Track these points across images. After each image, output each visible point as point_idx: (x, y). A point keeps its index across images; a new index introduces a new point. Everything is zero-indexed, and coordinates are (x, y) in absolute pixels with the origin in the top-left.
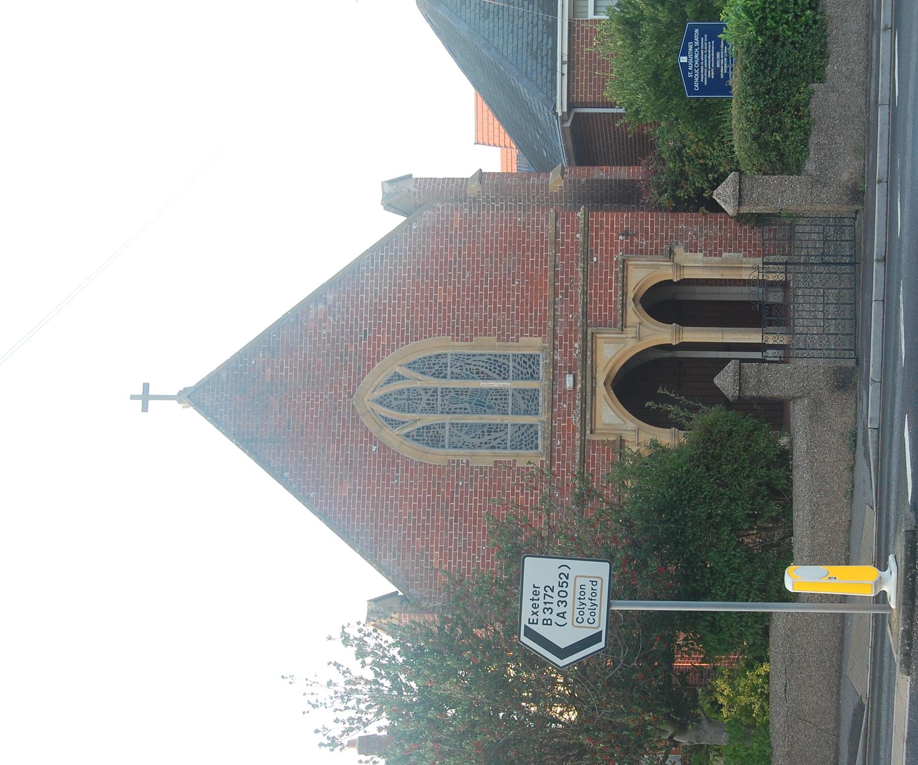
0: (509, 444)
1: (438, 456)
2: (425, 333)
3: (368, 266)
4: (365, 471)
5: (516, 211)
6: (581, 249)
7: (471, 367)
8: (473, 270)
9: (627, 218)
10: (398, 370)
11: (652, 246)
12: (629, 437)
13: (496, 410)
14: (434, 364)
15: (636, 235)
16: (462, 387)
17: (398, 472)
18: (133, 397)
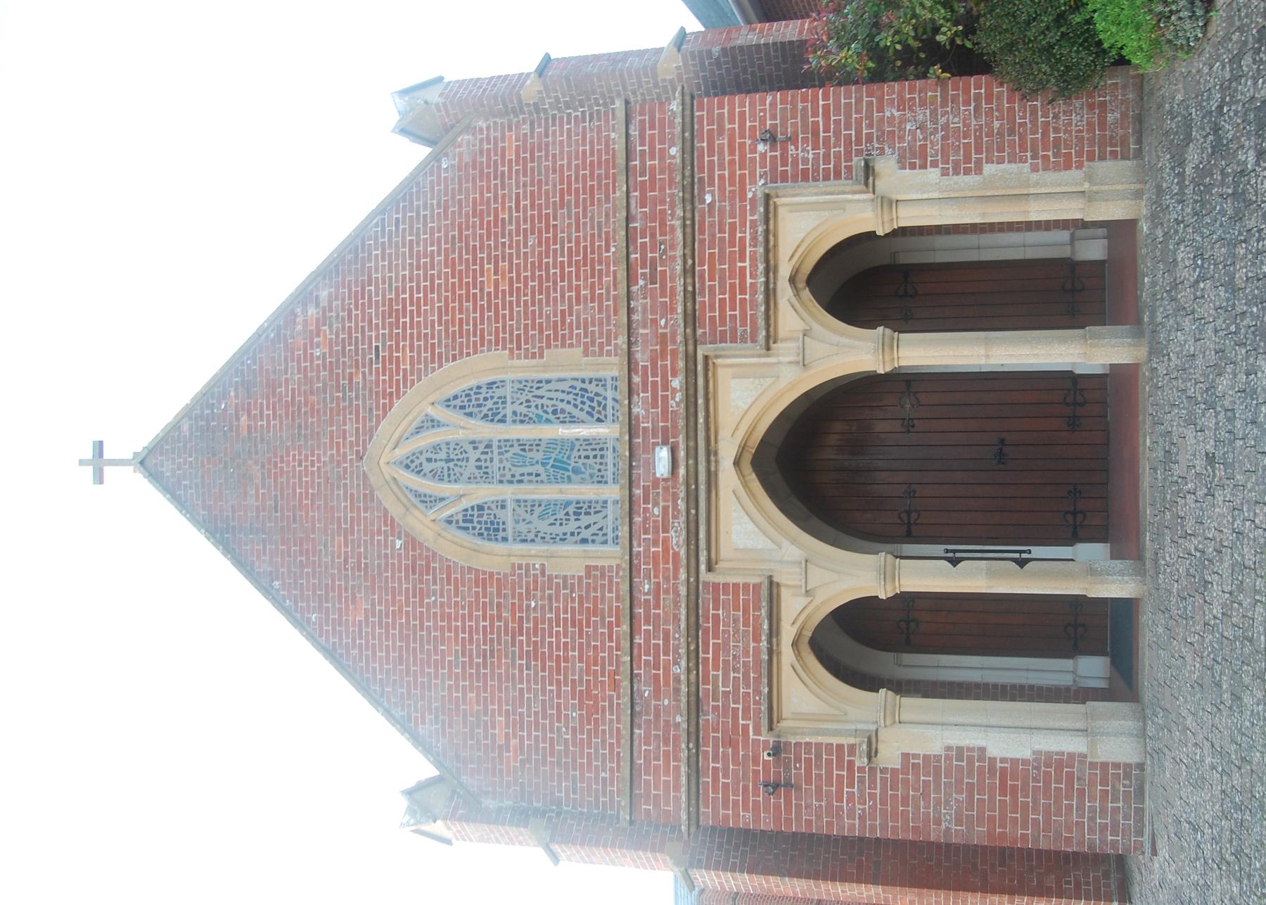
0: (610, 536)
1: (496, 557)
2: (468, 348)
3: (376, 239)
4: (387, 582)
5: (607, 121)
6: (678, 178)
7: (544, 401)
8: (540, 232)
9: (773, 105)
10: (430, 411)
11: (827, 159)
12: (788, 577)
13: (587, 476)
14: (486, 399)
15: (793, 139)
16: (532, 437)
17: (435, 583)
18: (82, 463)
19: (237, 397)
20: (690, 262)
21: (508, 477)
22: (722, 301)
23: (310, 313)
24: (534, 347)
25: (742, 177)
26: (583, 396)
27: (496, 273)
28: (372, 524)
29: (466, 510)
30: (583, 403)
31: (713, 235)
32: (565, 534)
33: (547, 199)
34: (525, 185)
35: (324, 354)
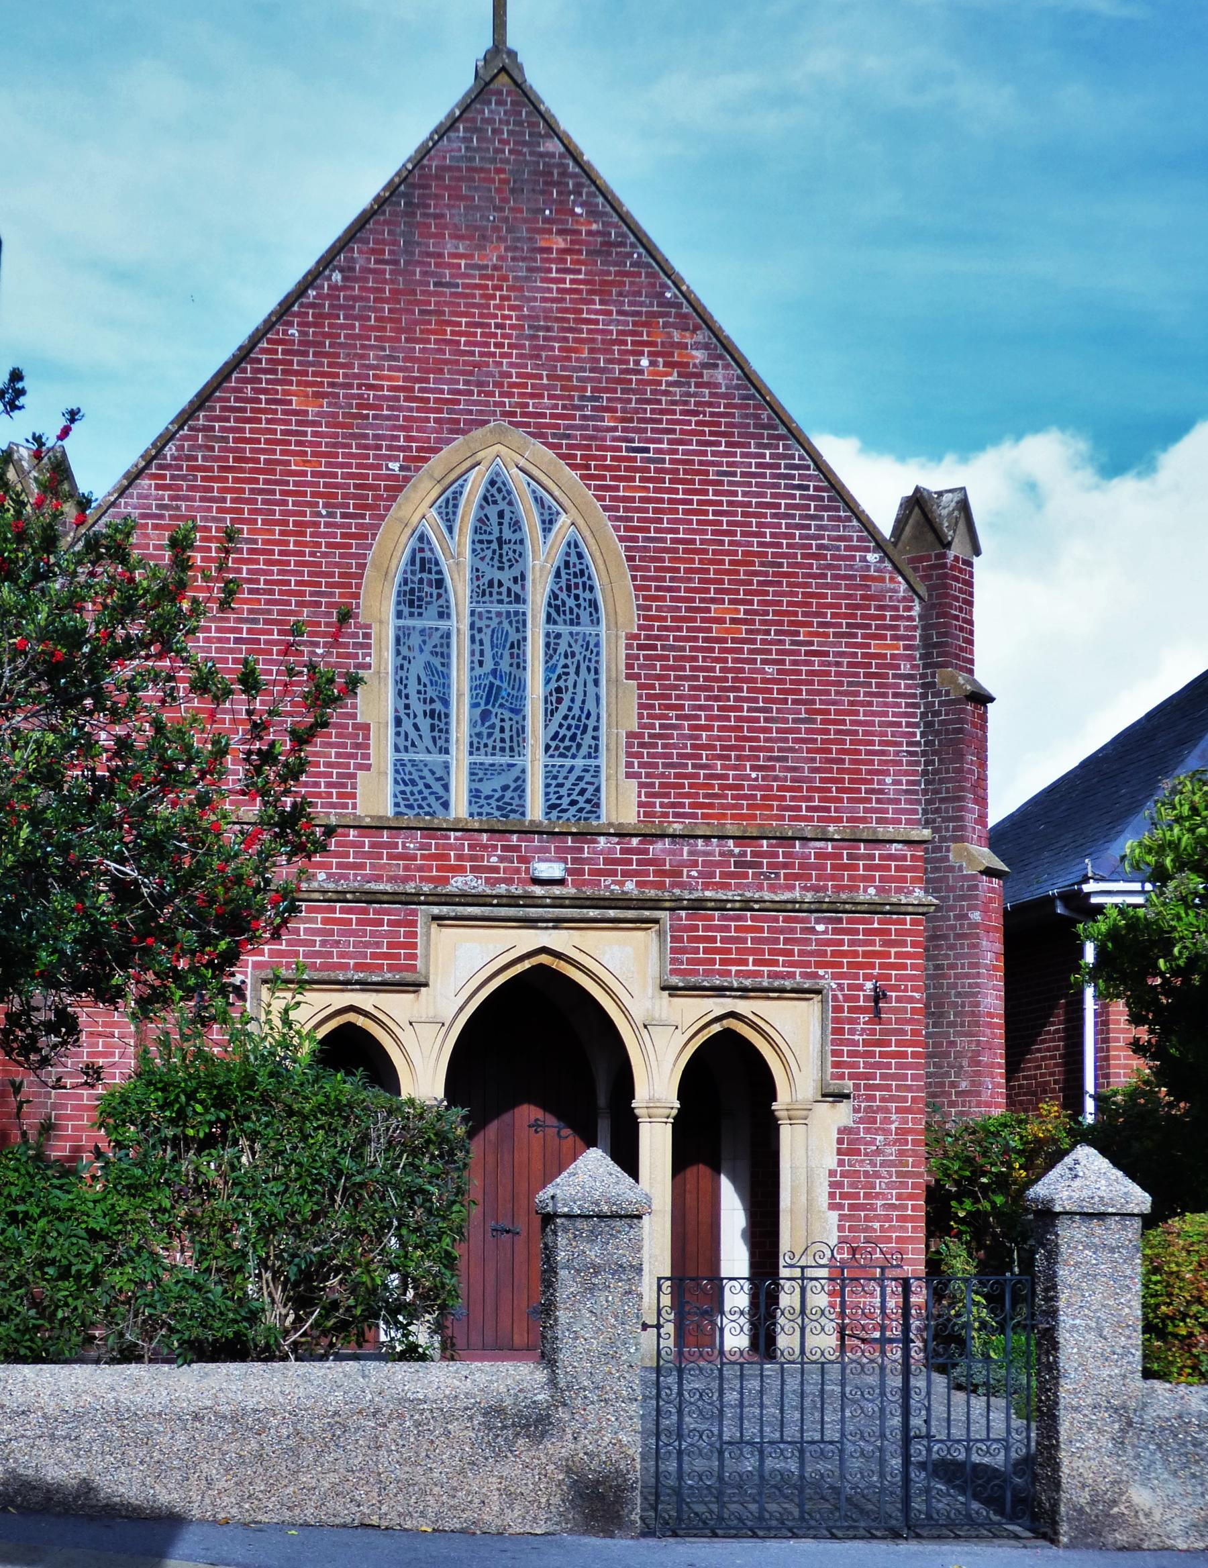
1: (380, 607)
6: (844, 896)
9: (911, 1000)
10: (563, 519)
14: (577, 597)
19: (589, 233)
20: (756, 906)
21: (478, 624)
22: (714, 940)
23: (694, 353)
24: (640, 667)
25: (840, 965)
26: (577, 727)
27: (733, 621)
28: (419, 430)
29: (437, 564)
30: (569, 728)
31: (782, 932)
32: (407, 697)
33: (819, 693)
34: (838, 664)
35: (641, 372)
